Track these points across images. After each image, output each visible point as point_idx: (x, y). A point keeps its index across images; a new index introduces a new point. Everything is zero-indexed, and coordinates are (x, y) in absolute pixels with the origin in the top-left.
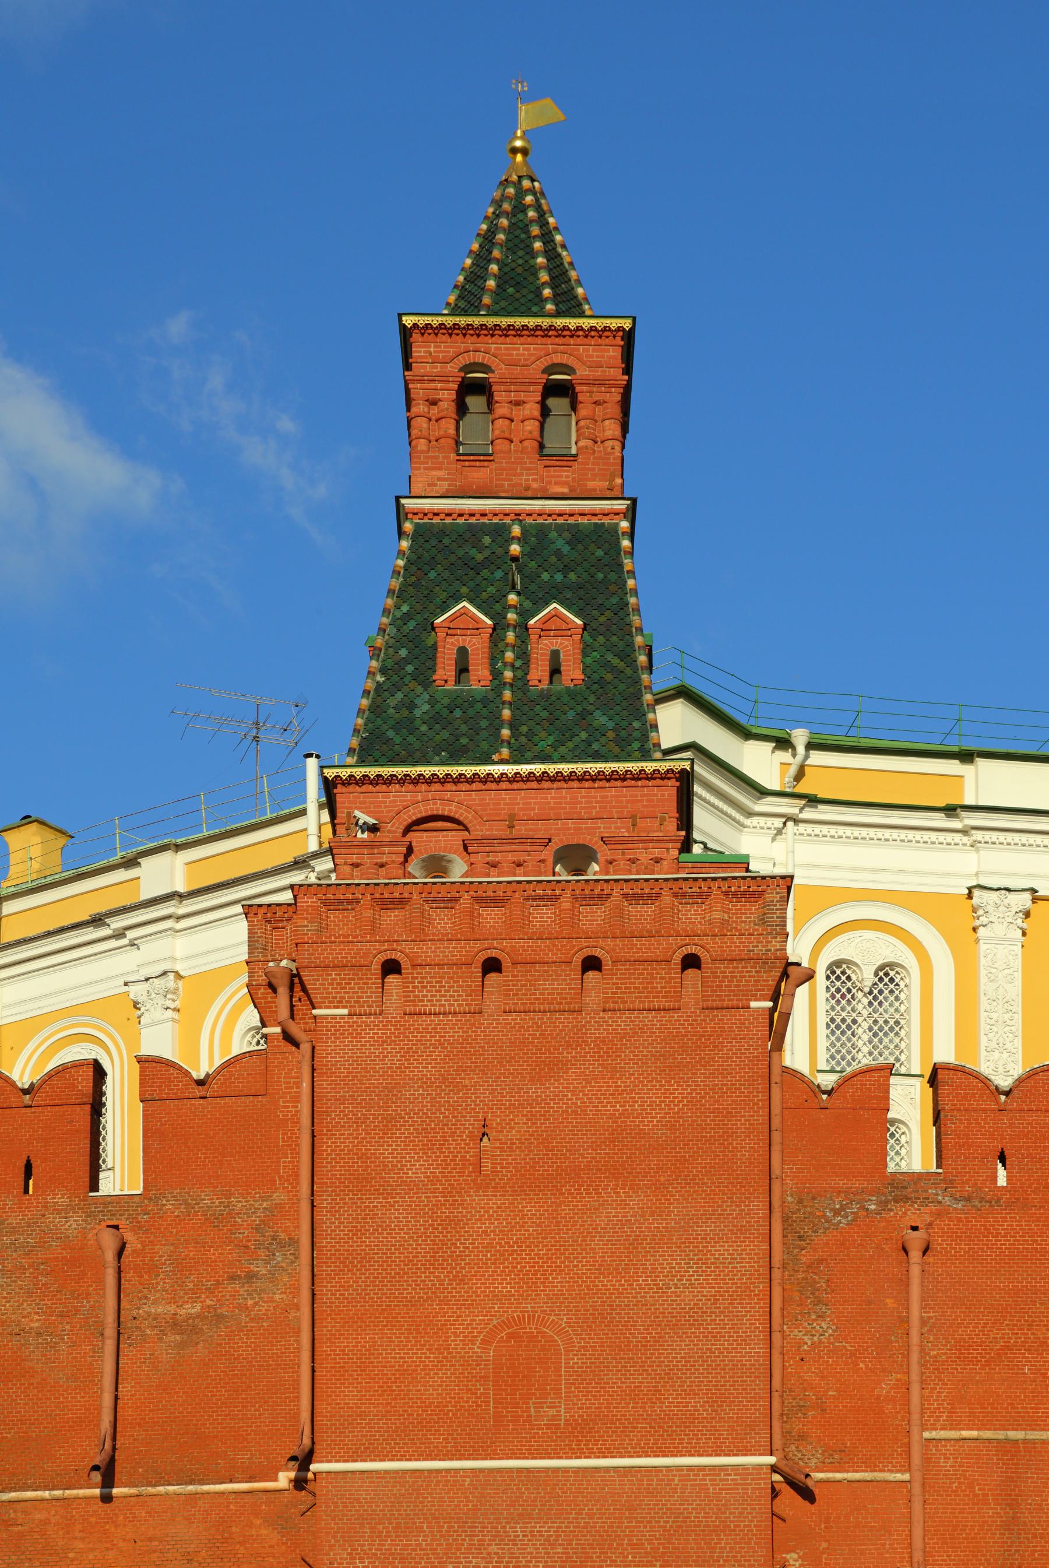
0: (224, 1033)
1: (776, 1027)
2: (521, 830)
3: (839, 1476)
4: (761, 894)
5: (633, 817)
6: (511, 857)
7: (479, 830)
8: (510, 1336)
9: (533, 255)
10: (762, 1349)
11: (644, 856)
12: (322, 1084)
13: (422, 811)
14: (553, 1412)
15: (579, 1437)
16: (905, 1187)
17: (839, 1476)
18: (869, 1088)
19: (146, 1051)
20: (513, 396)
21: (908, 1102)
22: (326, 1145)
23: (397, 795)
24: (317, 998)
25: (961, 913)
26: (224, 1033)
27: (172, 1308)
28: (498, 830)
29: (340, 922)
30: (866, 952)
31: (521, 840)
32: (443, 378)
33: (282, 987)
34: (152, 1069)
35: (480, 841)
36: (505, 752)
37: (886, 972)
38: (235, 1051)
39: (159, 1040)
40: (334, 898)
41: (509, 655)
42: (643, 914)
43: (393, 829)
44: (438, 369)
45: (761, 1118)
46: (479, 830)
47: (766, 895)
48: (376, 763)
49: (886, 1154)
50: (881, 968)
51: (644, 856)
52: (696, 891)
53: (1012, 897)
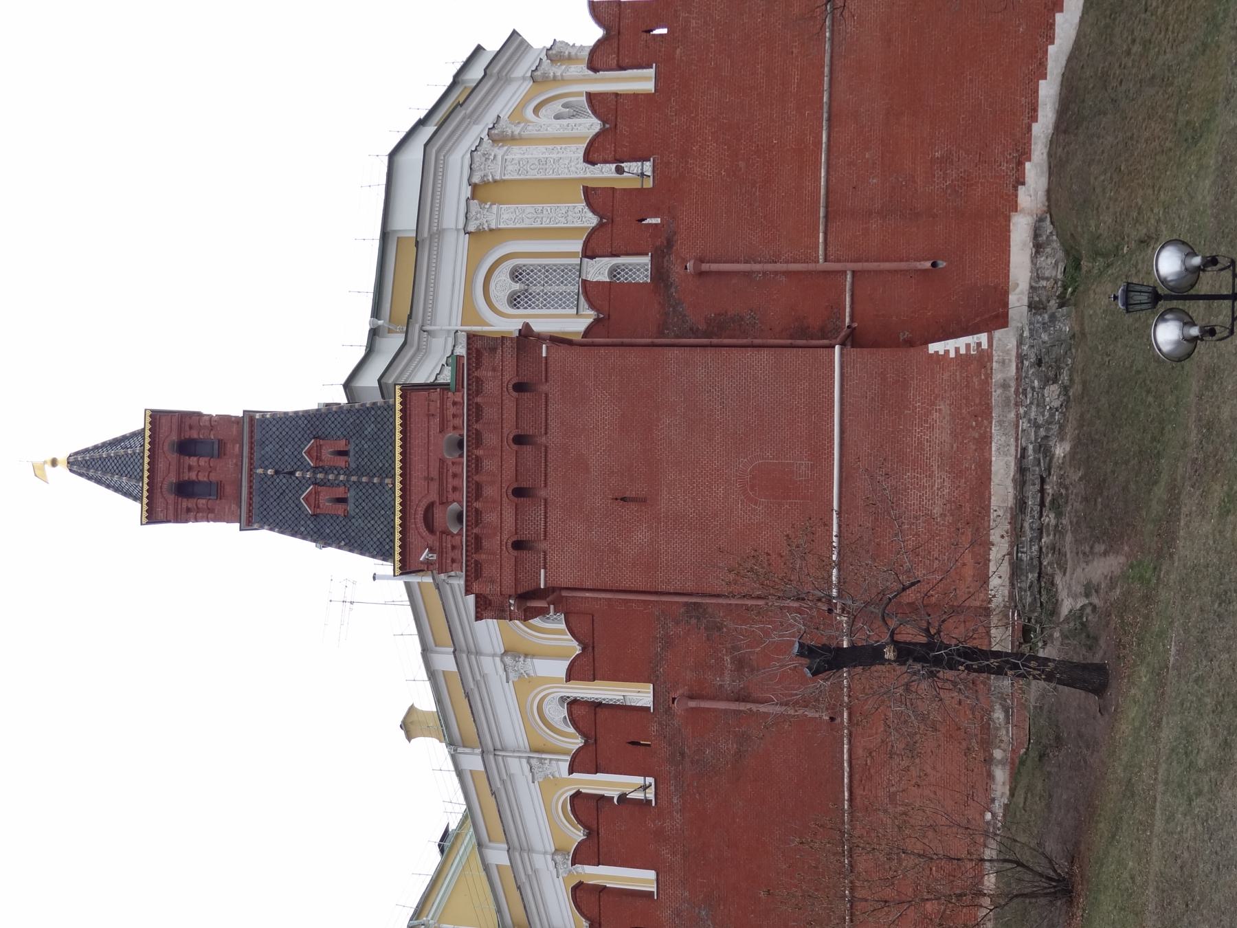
0: (553, 638)
1: (557, 340)
2: (434, 473)
3: (848, 310)
4: (477, 350)
5: (428, 415)
6: (450, 480)
7: (434, 496)
8: (752, 489)
9: (109, 457)
10: (765, 353)
11: (452, 410)
12: (588, 584)
13: (423, 529)
14: (803, 467)
15: (821, 454)
16: (659, 273)
17: (848, 310)
18: (589, 290)
19: (563, 675)
20: (186, 470)
21: (599, 270)
22: (626, 584)
23: (413, 539)
24: (533, 586)
25: (480, 237)
26: (553, 638)
27: (727, 672)
28: (434, 486)
29: (490, 570)
30: (503, 285)
31: (441, 473)
32: (176, 504)
33: (529, 602)
34: (572, 674)
35: (440, 494)
36: (388, 481)
37: (516, 275)
38: (563, 626)
39: (559, 668)
40: (474, 576)
41: (331, 477)
42: (490, 413)
43: (431, 539)
44: (171, 507)
45: (617, 351)
46: (434, 496)
47: (480, 348)
48: (393, 548)
49: (630, 283)
50: (513, 279)
51: (452, 410)
52: (476, 387)
53: (473, 213)
